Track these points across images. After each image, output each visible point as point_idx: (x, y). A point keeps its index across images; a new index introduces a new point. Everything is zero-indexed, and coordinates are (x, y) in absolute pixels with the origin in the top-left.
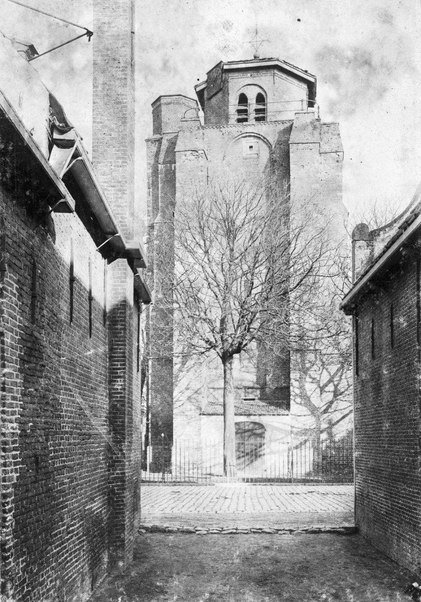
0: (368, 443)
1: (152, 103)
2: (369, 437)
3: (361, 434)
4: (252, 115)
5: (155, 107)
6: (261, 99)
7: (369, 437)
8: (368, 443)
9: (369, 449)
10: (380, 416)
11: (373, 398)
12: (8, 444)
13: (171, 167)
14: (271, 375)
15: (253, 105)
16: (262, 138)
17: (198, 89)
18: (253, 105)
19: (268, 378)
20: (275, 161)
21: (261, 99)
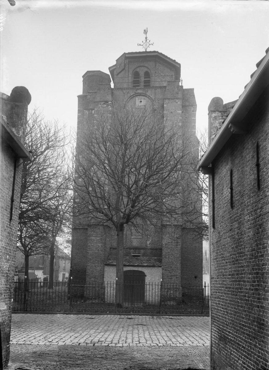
0: (225, 293)
1: (83, 75)
2: (227, 288)
3: (217, 284)
4: (142, 84)
5: (85, 77)
6: (147, 74)
7: (227, 288)
8: (225, 293)
9: (226, 300)
10: (242, 267)
11: (233, 248)
12: (264, 330)
13: (92, 112)
14: (150, 240)
15: (142, 79)
16: (148, 96)
17: (111, 69)
18: (142, 79)
19: (148, 243)
20: (155, 110)
21: (147, 74)
